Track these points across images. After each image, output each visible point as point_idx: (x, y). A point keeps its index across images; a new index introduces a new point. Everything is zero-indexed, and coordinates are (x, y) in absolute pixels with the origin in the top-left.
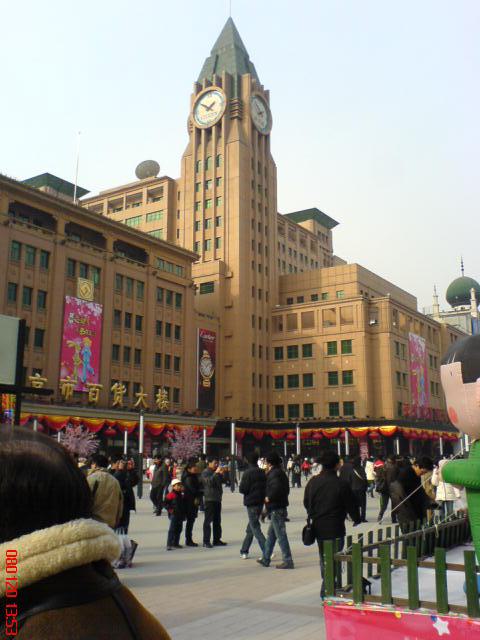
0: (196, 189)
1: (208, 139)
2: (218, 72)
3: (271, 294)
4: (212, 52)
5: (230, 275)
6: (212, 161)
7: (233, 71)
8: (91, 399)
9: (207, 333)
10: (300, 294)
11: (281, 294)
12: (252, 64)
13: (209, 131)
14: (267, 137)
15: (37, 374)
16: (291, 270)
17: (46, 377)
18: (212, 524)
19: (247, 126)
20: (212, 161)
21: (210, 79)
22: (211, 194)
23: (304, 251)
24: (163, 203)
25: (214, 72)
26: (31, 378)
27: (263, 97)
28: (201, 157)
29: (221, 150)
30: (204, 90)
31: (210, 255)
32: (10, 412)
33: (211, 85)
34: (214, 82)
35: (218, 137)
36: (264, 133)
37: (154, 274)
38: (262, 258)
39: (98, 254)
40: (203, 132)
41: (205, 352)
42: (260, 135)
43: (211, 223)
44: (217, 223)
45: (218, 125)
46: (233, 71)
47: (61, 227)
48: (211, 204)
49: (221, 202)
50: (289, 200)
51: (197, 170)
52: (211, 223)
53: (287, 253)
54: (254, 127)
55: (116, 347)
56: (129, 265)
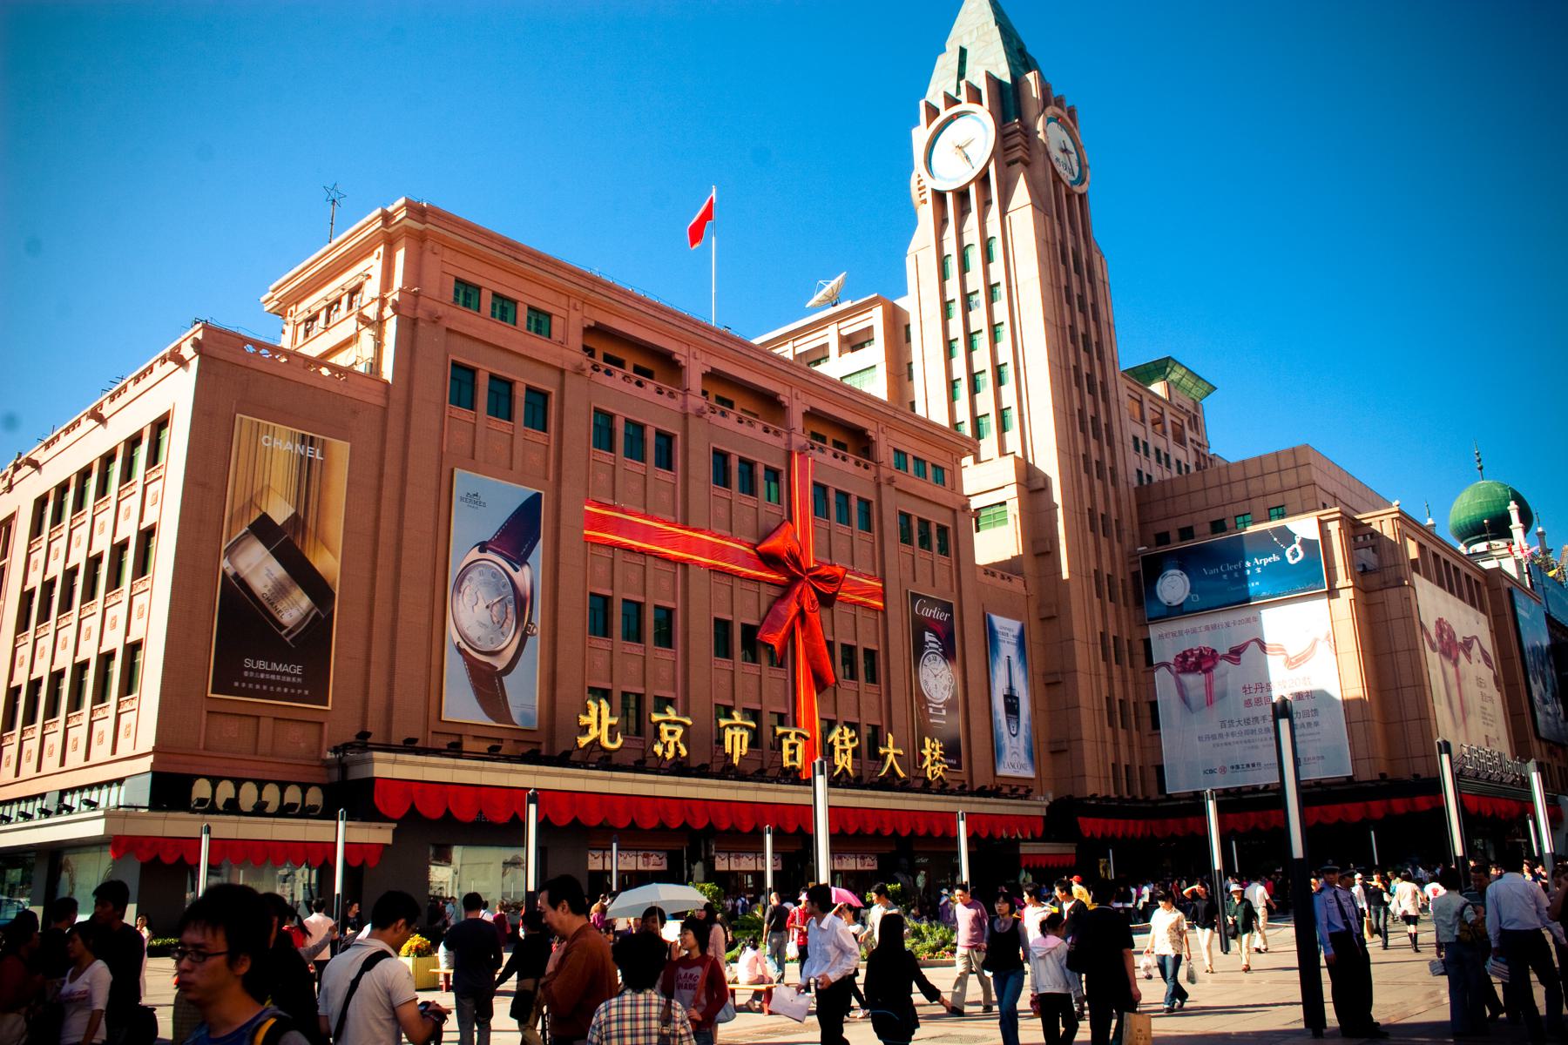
0: (943, 275)
1: (963, 211)
2: (968, 77)
3: (1126, 525)
5: (1041, 485)
6: (975, 256)
7: (1004, 74)
8: (787, 763)
9: (932, 602)
10: (1184, 523)
11: (1142, 524)
13: (962, 195)
14: (1082, 197)
15: (669, 709)
16: (1180, 471)
17: (686, 714)
18: (1062, 1029)
19: (1040, 172)
20: (975, 256)
21: (953, 93)
22: (975, 281)
23: (1162, 444)
24: (875, 353)
25: (961, 75)
26: (656, 717)
28: (950, 247)
29: (993, 228)
30: (944, 114)
31: (989, 445)
32: (681, 746)
33: (959, 102)
34: (963, 97)
35: (985, 203)
36: (1078, 189)
37: (891, 481)
38: (1101, 450)
39: (770, 438)
40: (949, 197)
41: (928, 636)
43: (987, 381)
44: (999, 380)
45: (983, 179)
46: (1004, 74)
47: (694, 381)
48: (982, 341)
49: (1005, 332)
50: (1131, 348)
51: (943, 275)
52: (987, 381)
53: (1153, 457)
55: (849, 651)
56: (838, 463)
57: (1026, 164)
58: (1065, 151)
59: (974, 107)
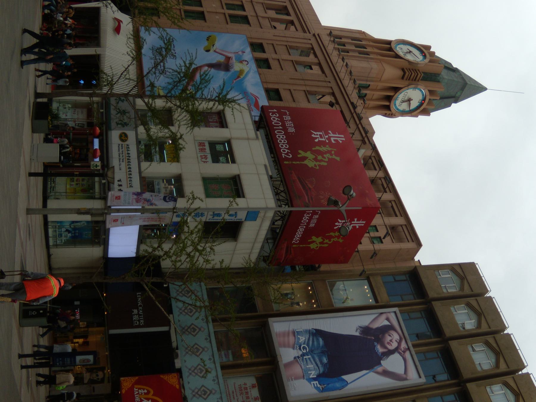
12: (450, 106)
13: (390, 49)
27: (423, 109)
42: (389, 98)
45: (397, 56)
54: (396, 90)
57: (403, 78)
58: (409, 100)
59: (427, 60)
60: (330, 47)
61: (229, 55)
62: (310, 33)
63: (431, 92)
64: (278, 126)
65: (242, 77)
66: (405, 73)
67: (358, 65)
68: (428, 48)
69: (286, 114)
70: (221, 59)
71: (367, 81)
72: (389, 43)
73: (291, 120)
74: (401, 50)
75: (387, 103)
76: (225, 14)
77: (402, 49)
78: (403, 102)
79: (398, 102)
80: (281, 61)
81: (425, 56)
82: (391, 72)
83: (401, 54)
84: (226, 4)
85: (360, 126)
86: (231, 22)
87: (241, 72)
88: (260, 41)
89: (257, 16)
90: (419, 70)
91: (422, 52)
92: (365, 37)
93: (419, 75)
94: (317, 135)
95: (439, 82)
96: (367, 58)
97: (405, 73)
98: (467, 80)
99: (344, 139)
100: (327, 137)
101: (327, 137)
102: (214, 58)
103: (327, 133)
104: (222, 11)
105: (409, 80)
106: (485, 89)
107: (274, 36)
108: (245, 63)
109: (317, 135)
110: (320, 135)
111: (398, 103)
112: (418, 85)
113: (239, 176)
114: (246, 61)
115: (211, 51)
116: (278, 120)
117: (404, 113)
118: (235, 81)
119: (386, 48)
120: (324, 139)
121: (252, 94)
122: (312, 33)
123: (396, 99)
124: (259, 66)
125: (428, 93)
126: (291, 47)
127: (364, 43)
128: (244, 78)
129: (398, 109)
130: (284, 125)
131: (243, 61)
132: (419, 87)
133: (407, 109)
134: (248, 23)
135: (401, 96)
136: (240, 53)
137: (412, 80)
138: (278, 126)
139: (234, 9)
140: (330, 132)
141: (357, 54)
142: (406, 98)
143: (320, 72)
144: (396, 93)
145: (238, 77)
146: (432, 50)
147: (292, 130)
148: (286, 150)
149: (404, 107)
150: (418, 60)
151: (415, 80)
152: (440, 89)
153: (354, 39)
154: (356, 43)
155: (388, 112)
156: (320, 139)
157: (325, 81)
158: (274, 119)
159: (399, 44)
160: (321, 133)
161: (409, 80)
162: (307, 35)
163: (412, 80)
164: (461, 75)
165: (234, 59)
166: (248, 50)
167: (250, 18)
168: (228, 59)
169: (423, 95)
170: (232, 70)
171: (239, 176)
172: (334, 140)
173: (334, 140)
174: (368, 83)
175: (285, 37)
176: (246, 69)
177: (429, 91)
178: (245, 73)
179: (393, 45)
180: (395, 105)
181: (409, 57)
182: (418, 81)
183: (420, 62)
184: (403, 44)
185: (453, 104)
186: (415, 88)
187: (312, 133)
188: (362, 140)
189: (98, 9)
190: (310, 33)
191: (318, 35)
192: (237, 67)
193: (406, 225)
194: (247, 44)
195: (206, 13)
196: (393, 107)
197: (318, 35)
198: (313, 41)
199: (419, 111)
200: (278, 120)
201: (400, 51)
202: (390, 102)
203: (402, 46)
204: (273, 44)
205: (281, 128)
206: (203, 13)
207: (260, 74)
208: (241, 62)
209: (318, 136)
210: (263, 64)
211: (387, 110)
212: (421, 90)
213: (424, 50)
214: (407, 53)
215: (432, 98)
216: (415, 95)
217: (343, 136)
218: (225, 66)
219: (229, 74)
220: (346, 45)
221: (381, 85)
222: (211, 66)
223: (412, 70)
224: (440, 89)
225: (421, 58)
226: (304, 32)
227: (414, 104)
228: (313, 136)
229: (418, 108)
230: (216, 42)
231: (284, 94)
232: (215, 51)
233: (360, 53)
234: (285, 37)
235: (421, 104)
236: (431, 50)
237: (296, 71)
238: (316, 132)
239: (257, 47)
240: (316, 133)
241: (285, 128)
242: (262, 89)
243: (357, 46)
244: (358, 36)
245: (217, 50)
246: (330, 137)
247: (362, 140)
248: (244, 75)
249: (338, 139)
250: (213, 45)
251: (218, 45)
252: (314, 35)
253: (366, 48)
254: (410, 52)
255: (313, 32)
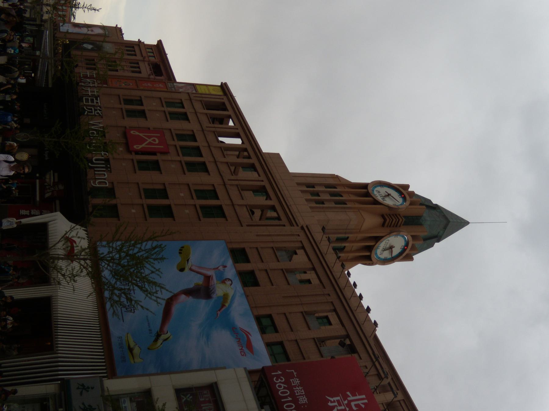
4: (436, 205)
12: (432, 245)
13: (368, 195)
27: (406, 255)
42: (370, 249)
45: (376, 202)
54: (378, 239)
57: (383, 225)
58: (391, 248)
59: (408, 203)
60: (325, 246)
61: (209, 273)
62: (298, 226)
63: (414, 237)
64: (286, 397)
65: (227, 305)
66: (385, 220)
67: (336, 218)
68: (406, 187)
69: (293, 377)
70: (199, 280)
71: (345, 233)
72: (365, 186)
73: (301, 385)
74: (379, 193)
75: (368, 254)
76: (175, 146)
77: (379, 192)
78: (385, 250)
79: (379, 251)
80: (269, 271)
81: (404, 199)
82: (370, 221)
83: (380, 199)
84: (177, 135)
85: (377, 363)
86: (189, 171)
87: (225, 297)
88: (242, 246)
89: (233, 205)
90: (399, 215)
91: (401, 193)
92: (339, 183)
93: (401, 220)
94: (334, 402)
95: (421, 225)
96: (344, 208)
97: (385, 220)
98: (449, 217)
99: (366, 401)
100: (346, 402)
101: (346, 402)
102: (192, 280)
103: (345, 397)
104: (163, 109)
105: (390, 226)
106: (467, 223)
107: (257, 235)
108: (229, 283)
109: (334, 402)
110: (338, 401)
111: (380, 251)
112: (401, 231)
113: (216, 383)
114: (229, 280)
115: (187, 270)
116: (285, 388)
117: (385, 262)
118: (219, 312)
119: (363, 191)
120: (343, 407)
121: (242, 330)
122: (300, 226)
123: (377, 248)
124: (245, 284)
125: (410, 239)
126: (279, 249)
127: (338, 189)
128: (230, 306)
129: (379, 258)
130: (292, 395)
131: (226, 279)
132: (402, 233)
133: (389, 256)
134: (223, 216)
135: (383, 244)
136: (221, 268)
137: (393, 226)
138: (286, 397)
139: (206, 198)
140: (348, 393)
141: (333, 205)
142: (388, 246)
143: (306, 259)
144: (377, 242)
145: (223, 306)
146: (410, 190)
147: (303, 400)
148: (282, 385)
149: (386, 255)
150: (398, 204)
151: (396, 226)
152: (422, 232)
153: (328, 186)
154: (329, 190)
155: (370, 262)
156: (339, 408)
157: (324, 295)
158: (280, 386)
159: (375, 187)
160: (338, 398)
161: (390, 226)
162: (296, 229)
163: (393, 226)
164: (442, 212)
165: (214, 278)
166: (230, 263)
167: (208, 165)
168: (208, 278)
169: (405, 241)
170: (214, 296)
171: (216, 383)
172: (356, 405)
173: (356, 405)
174: (347, 236)
175: (270, 235)
176: (231, 293)
177: (412, 236)
178: (230, 298)
179: (370, 189)
180: (376, 254)
181: (389, 202)
182: (400, 226)
183: (401, 207)
184: (380, 186)
185: (436, 244)
186: (397, 235)
187: (329, 400)
188: (377, 375)
189: (44, 227)
190: (298, 226)
191: (307, 226)
192: (220, 290)
193: (403, 400)
194: (228, 254)
195: (147, 112)
196: (374, 257)
197: (307, 226)
198: (302, 237)
199: (401, 257)
200: (285, 388)
201: (378, 194)
202: (371, 251)
203: (378, 188)
204: (257, 248)
205: (290, 399)
206: (169, 207)
207: (247, 296)
208: (223, 282)
209: (336, 404)
210: (249, 279)
211: (368, 260)
212: (403, 237)
213: (402, 190)
214: (386, 196)
215: (415, 242)
216: (397, 242)
217: (364, 396)
218: (203, 291)
219: (212, 302)
220: (320, 194)
221: (360, 236)
222: (188, 292)
223: (393, 215)
224: (422, 232)
225: (400, 200)
226: (292, 225)
227: (396, 251)
228: (330, 404)
229: (400, 254)
230: (191, 256)
231: (280, 322)
232: (191, 269)
233: (337, 203)
234: (270, 235)
235: (404, 250)
236: (410, 190)
237: (289, 284)
238: (332, 397)
239: (239, 255)
240: (332, 399)
241: (295, 400)
242: (252, 316)
243: (333, 194)
244: (331, 181)
245: (193, 268)
246: (350, 402)
247: (377, 375)
248: (229, 301)
249: (359, 402)
250: (188, 261)
251: (194, 259)
252: (302, 228)
253: (346, 204)
254: (389, 195)
255: (301, 222)
